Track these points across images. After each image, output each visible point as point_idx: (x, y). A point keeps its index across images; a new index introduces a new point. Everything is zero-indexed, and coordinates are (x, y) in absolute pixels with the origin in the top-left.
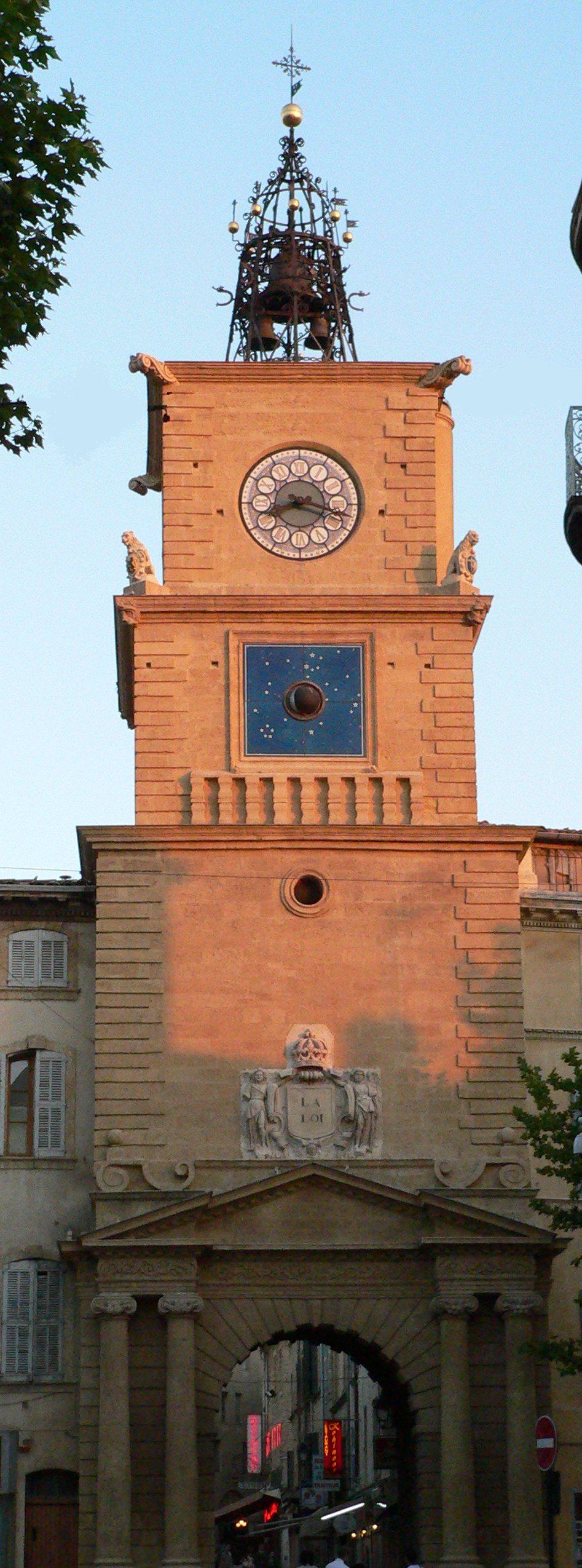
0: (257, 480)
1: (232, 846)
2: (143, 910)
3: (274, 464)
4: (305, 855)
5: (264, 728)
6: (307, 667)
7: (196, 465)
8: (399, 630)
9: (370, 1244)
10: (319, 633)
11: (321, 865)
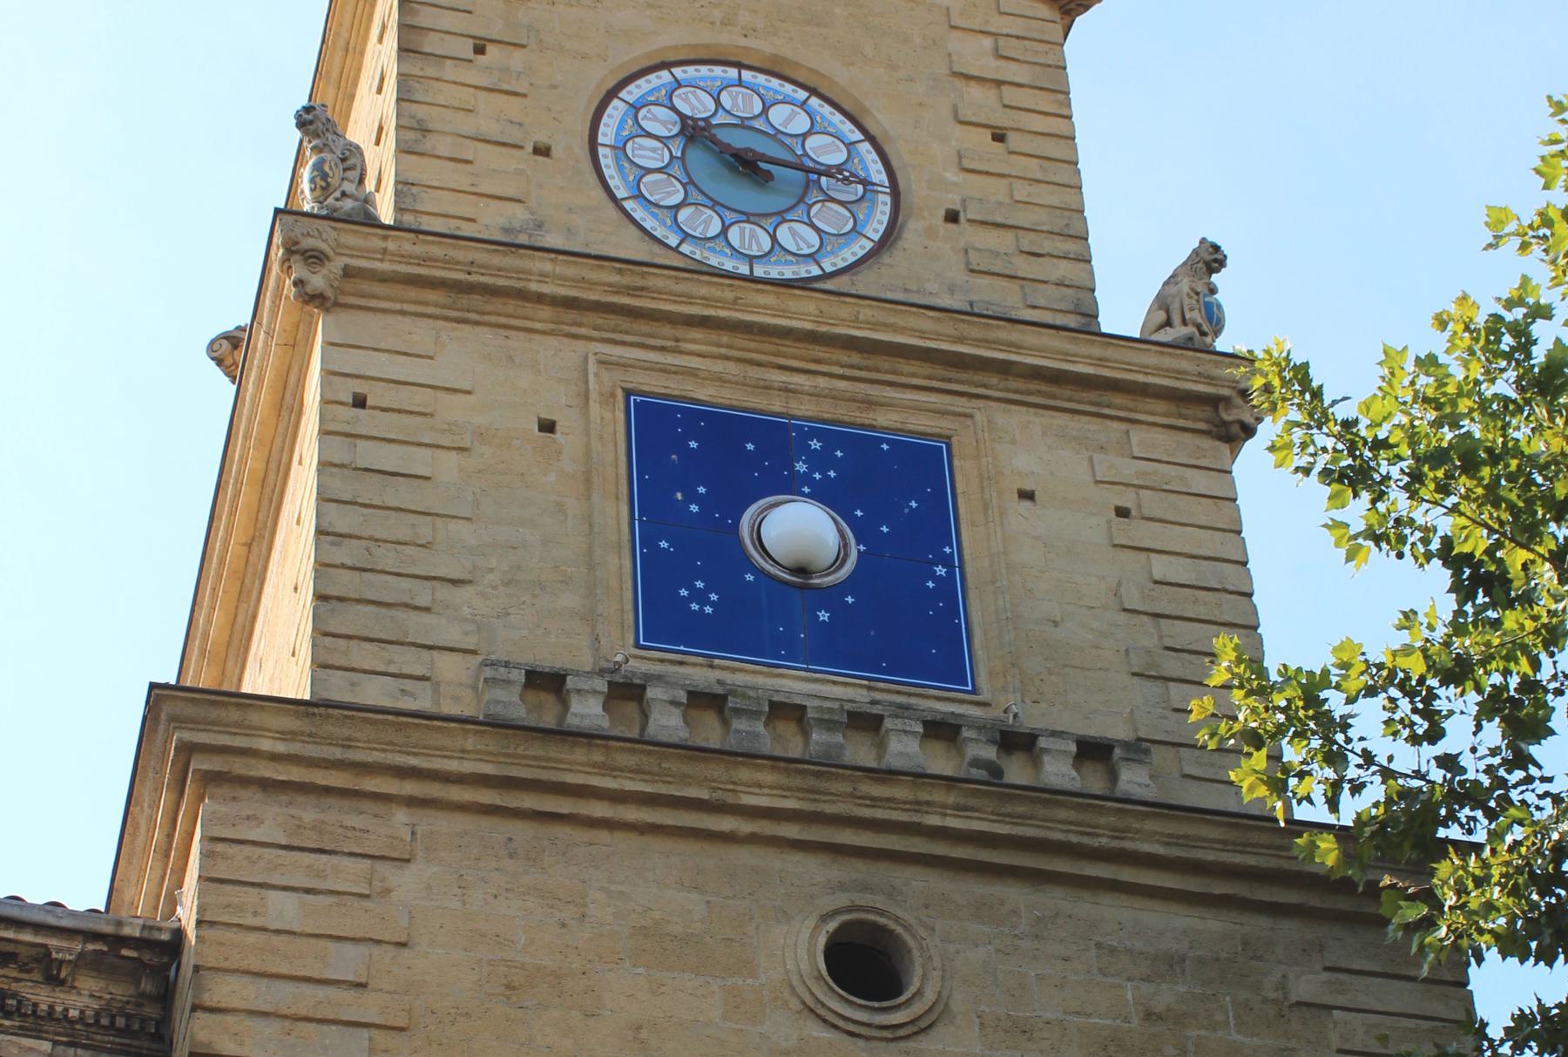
0: (635, 108)
1: (631, 814)
2: (346, 962)
3: (679, 84)
4: (859, 870)
5: (691, 588)
6: (801, 467)
7: (480, 50)
8: (1038, 421)
9: (1379, 969)
10: (834, 396)
11: (914, 903)
